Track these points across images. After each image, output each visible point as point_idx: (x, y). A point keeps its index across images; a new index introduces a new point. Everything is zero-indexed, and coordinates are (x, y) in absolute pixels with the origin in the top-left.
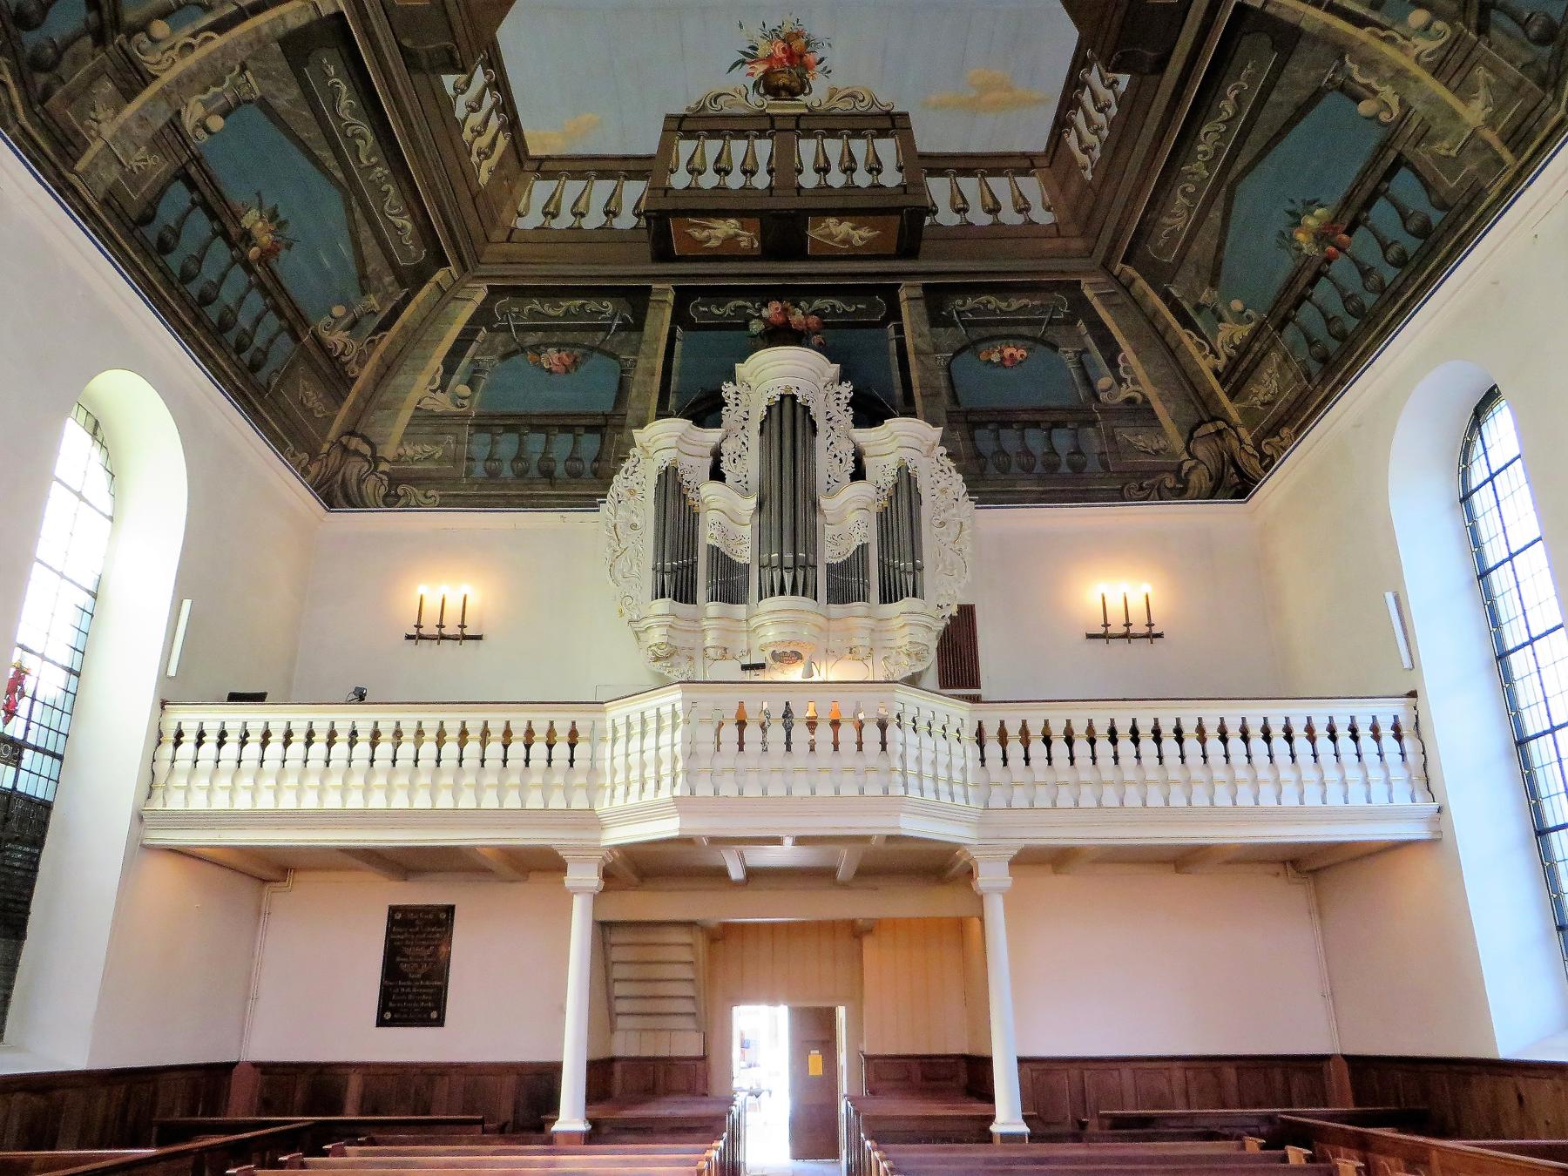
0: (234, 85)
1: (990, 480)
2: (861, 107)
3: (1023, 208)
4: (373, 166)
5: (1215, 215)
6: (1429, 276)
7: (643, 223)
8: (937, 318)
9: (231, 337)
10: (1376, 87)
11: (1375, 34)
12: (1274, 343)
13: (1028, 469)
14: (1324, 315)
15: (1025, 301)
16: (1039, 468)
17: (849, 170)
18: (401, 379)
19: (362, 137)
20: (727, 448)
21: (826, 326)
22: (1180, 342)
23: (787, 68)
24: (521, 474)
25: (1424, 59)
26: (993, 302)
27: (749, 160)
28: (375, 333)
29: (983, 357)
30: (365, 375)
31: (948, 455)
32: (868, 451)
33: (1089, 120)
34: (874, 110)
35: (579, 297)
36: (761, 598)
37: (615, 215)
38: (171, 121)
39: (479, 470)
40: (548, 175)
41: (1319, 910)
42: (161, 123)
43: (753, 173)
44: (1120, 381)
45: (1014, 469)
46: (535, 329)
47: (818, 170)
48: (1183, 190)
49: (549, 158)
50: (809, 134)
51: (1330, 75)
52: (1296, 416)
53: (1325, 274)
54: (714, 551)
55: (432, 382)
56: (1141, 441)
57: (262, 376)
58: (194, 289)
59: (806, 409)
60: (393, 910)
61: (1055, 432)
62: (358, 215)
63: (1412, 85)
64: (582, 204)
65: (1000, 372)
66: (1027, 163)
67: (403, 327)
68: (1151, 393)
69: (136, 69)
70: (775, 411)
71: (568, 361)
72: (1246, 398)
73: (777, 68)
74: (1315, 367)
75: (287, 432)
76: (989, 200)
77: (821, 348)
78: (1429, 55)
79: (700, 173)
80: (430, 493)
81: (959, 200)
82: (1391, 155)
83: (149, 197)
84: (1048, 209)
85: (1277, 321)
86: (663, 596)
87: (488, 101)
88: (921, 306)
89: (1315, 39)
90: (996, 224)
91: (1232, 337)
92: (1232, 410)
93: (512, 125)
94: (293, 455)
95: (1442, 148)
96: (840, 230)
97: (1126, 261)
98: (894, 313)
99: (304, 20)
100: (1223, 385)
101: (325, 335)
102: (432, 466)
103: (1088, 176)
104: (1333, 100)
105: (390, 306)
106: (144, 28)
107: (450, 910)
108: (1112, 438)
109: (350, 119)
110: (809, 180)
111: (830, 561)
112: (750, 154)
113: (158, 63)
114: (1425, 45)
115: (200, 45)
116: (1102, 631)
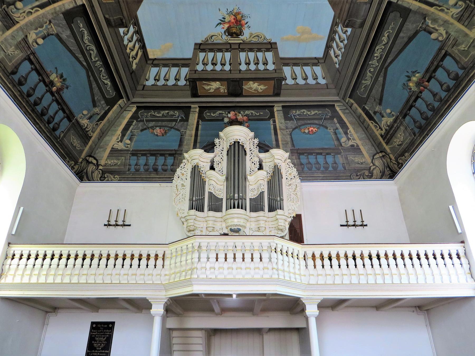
1: (306, 173)
2: (261, 40)
3: (316, 78)
4: (97, 61)
5: (381, 79)
6: (459, 93)
7: (188, 83)
8: (287, 118)
9: (46, 118)
10: (437, 28)
11: (437, 9)
12: (401, 123)
13: (319, 169)
14: (420, 111)
15: (316, 112)
16: (322, 169)
17: (257, 64)
18: (107, 138)
19: (93, 50)
22: (369, 125)
23: (235, 27)
24: (147, 170)
25: (455, 16)
26: (305, 111)
27: (223, 60)
28: (98, 121)
29: (303, 131)
30: (95, 136)
32: (264, 161)
34: (265, 41)
35: (167, 110)
36: (227, 210)
37: (179, 80)
38: (24, 38)
39: (133, 169)
40: (156, 66)
41: (430, 324)
42: (20, 39)
43: (224, 65)
45: (314, 169)
46: (152, 121)
47: (246, 64)
48: (370, 71)
49: (155, 59)
50: (243, 50)
51: (421, 25)
52: (411, 148)
53: (420, 97)
54: (210, 194)
57: (57, 133)
58: (32, 99)
59: (243, 146)
60: (93, 323)
61: (327, 156)
62: (92, 78)
63: (450, 26)
64: (167, 76)
65: (308, 136)
66: (316, 61)
67: (108, 119)
68: (359, 143)
69: (11, 19)
70: (232, 147)
71: (163, 132)
72: (392, 144)
73: (232, 26)
74: (417, 130)
75: (66, 154)
76: (304, 75)
77: (248, 127)
78: (457, 14)
79: (207, 65)
80: (115, 177)
81: (294, 75)
82: (443, 52)
83: (15, 64)
84: (324, 78)
85: (403, 115)
86: (192, 209)
87: (135, 38)
88: (281, 114)
89: (416, 12)
90: (307, 84)
92: (387, 148)
93: (143, 47)
94: (68, 162)
95: (462, 47)
96: (254, 86)
98: (272, 116)
99: (71, 6)
100: (384, 140)
101: (80, 120)
102: (116, 167)
103: (337, 66)
104: (422, 34)
105: (103, 112)
107: (113, 323)
108: (347, 158)
109: (88, 44)
110: (243, 67)
113: (19, 17)
114: (455, 11)
115: (34, 12)
116: (345, 224)
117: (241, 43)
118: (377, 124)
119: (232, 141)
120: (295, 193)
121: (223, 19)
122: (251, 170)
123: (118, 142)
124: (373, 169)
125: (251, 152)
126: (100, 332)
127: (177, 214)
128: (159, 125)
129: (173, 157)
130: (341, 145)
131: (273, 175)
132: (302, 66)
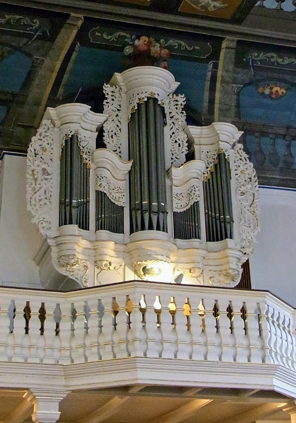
8: (240, 62)
13: (275, 165)
16: (281, 164)
20: (106, 127)
26: (275, 57)
29: (260, 90)
31: (244, 150)
32: (196, 140)
36: (132, 232)
98: (215, 55)
111: (175, 210)
119: (143, 96)
120: (252, 209)
122: (174, 157)
125: (173, 120)
127: (38, 230)
131: (213, 170)
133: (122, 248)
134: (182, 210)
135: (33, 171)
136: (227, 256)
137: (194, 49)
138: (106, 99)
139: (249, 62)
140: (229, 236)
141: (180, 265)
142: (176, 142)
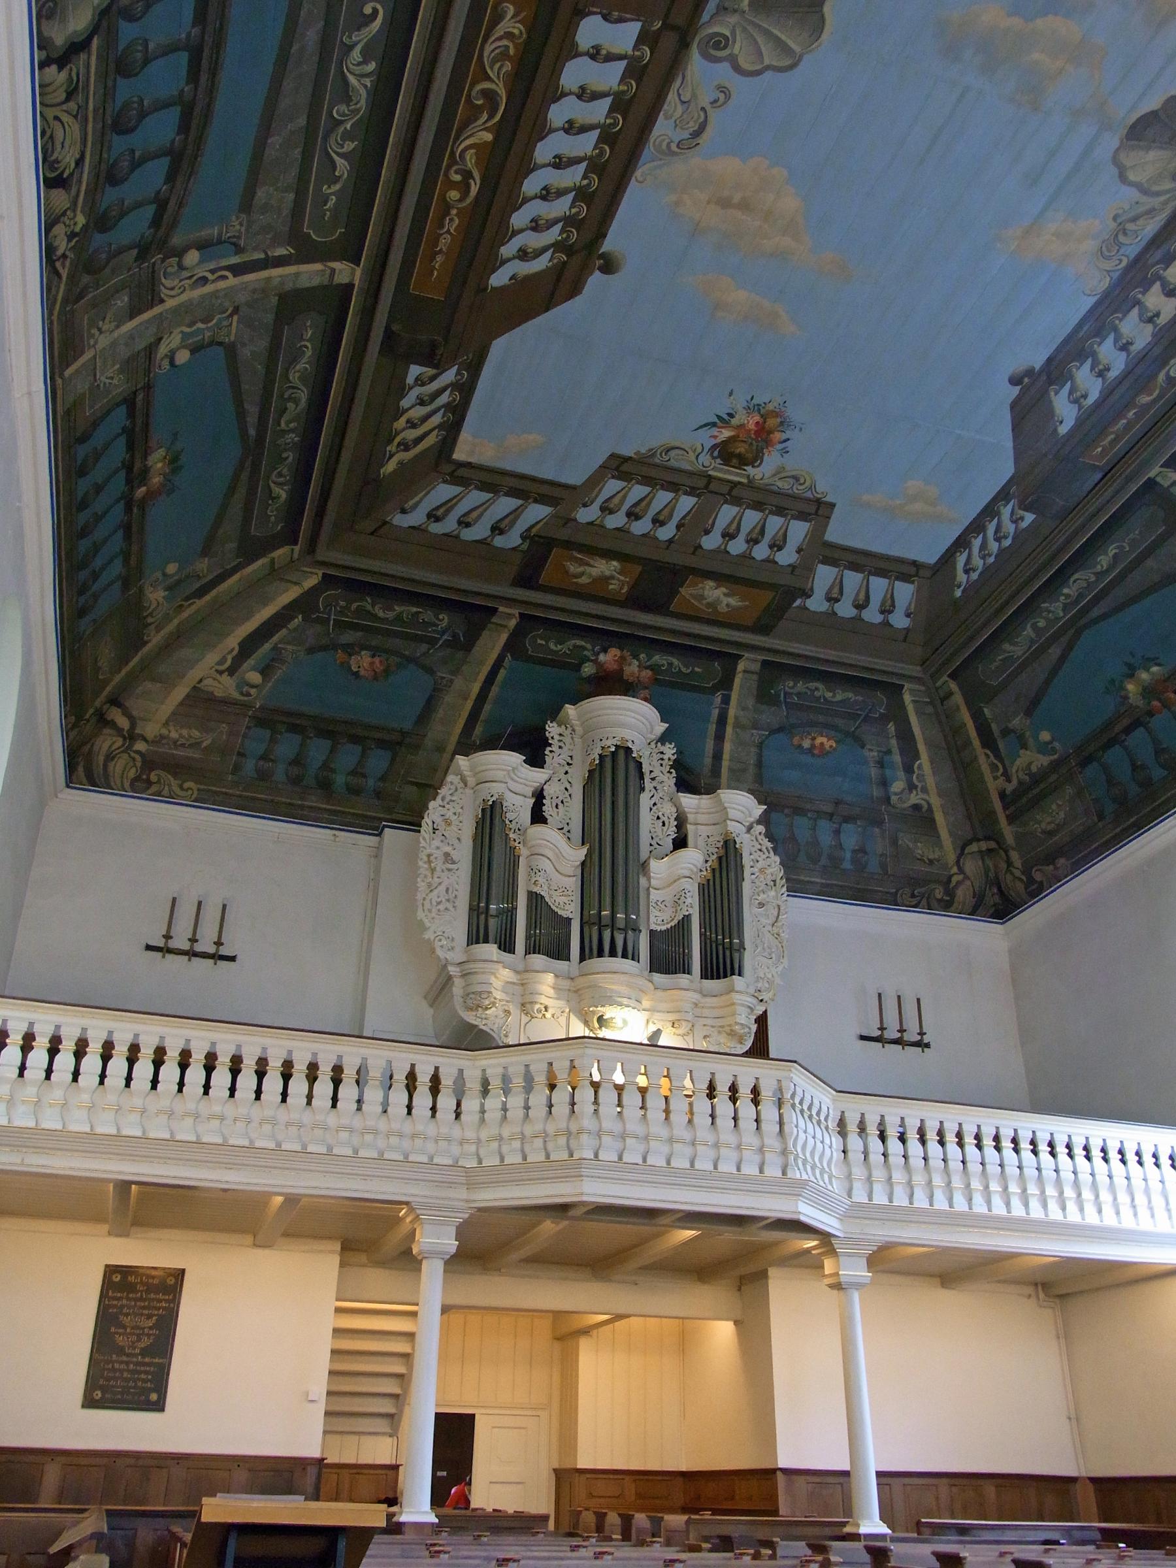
0: (218, 326)
2: (797, 490)
5: (1055, 652)
8: (765, 695)
15: (850, 695)
16: (824, 861)
19: (296, 402)
20: (549, 791)
21: (656, 681)
26: (821, 690)
29: (796, 740)
30: (155, 639)
32: (691, 818)
33: (984, 546)
34: (809, 495)
39: (250, 765)
41: (1066, 1336)
44: (911, 787)
46: (355, 627)
48: (1035, 627)
53: (1145, 725)
55: (224, 659)
56: (921, 849)
60: (110, 1270)
66: (913, 570)
68: (935, 801)
71: (379, 667)
76: (862, 596)
80: (186, 785)
84: (908, 616)
86: (486, 941)
87: (444, 398)
90: (858, 619)
91: (1030, 764)
92: (1008, 832)
96: (714, 594)
97: (953, 676)
98: (726, 683)
100: (1005, 808)
103: (958, 593)
106: (180, 253)
107: (183, 1271)
108: (894, 842)
112: (671, 507)
113: (172, 289)
116: (877, 1033)
117: (740, 483)
118: (1001, 760)
119: (609, 743)
120: (775, 930)
121: (726, 417)
123: (221, 673)
124: (959, 883)
126: (136, 1300)
127: (433, 951)
128: (373, 643)
129: (389, 754)
130: (888, 799)
131: (716, 866)
132: (870, 573)
133: (566, 984)
134: (664, 928)
135: (429, 856)
136: (733, 1004)
137: (693, 670)
138: (550, 745)
139: (779, 696)
140: (737, 971)
141: (657, 1015)
142: (658, 818)
